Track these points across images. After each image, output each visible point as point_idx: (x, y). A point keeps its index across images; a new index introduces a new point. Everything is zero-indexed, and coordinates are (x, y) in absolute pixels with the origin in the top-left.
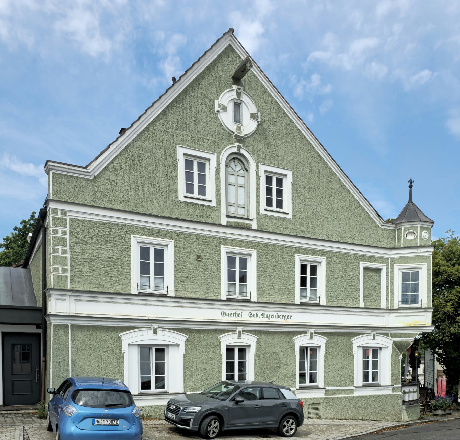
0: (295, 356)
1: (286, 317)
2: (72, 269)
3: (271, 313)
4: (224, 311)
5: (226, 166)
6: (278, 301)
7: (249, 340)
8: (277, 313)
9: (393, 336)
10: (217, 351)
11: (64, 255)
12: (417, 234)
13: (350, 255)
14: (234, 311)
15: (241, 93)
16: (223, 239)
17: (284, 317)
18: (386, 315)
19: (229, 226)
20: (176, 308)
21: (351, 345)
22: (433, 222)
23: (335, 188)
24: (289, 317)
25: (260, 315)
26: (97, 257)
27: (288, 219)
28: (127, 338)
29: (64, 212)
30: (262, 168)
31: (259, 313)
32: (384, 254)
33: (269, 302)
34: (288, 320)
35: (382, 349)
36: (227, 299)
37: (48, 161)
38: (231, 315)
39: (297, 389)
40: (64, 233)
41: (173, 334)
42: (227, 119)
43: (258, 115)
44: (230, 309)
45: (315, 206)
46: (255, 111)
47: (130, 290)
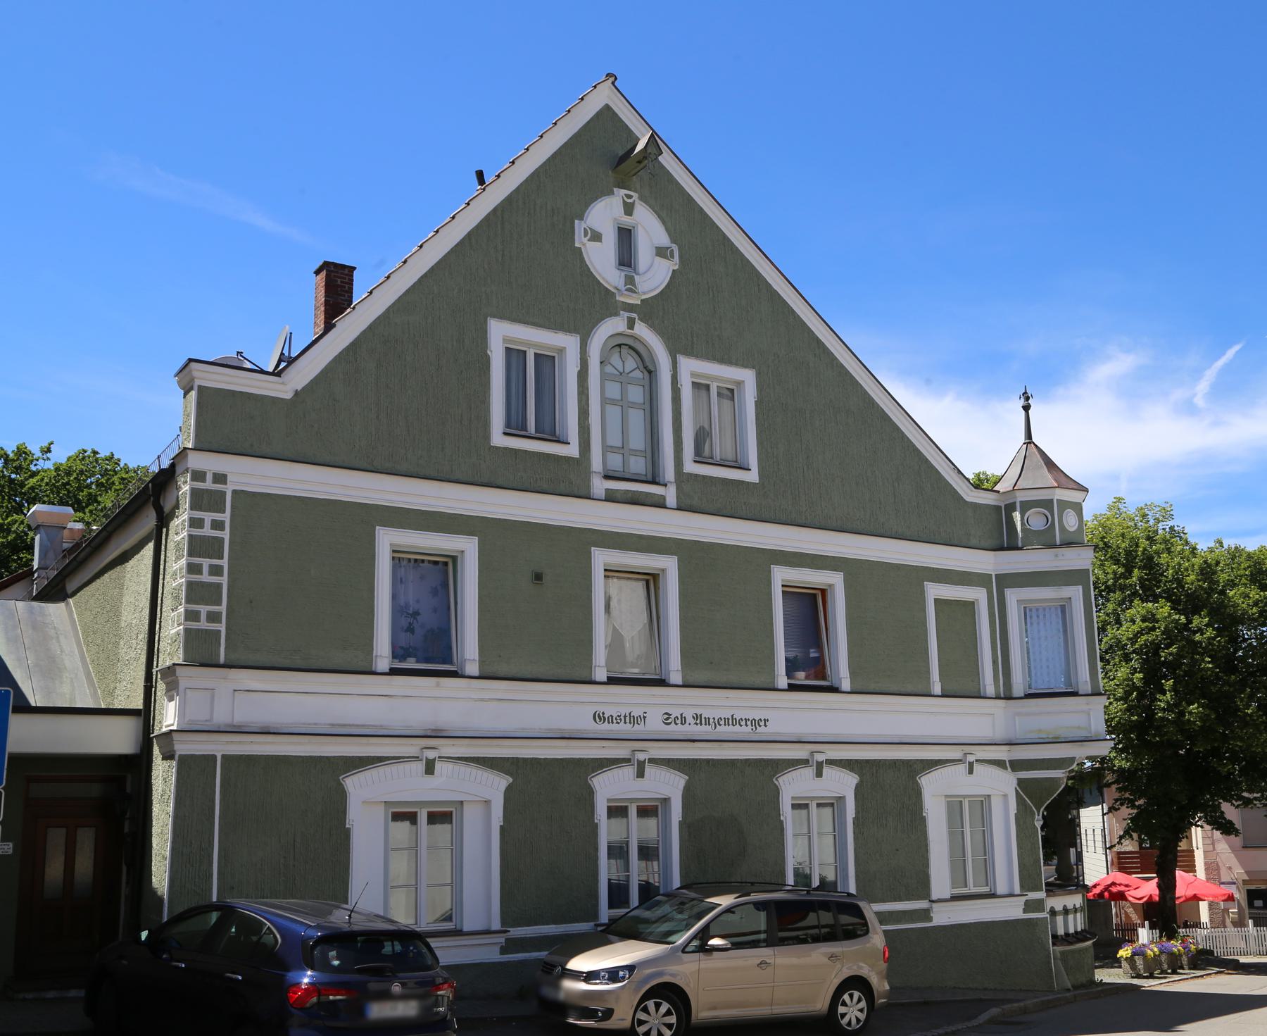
15: (633, 204)
19: (611, 497)
22: (1086, 490)
25: (690, 720)
29: (220, 478)
30: (690, 367)
36: (609, 678)
40: (216, 570)
42: (601, 260)
46: (663, 239)
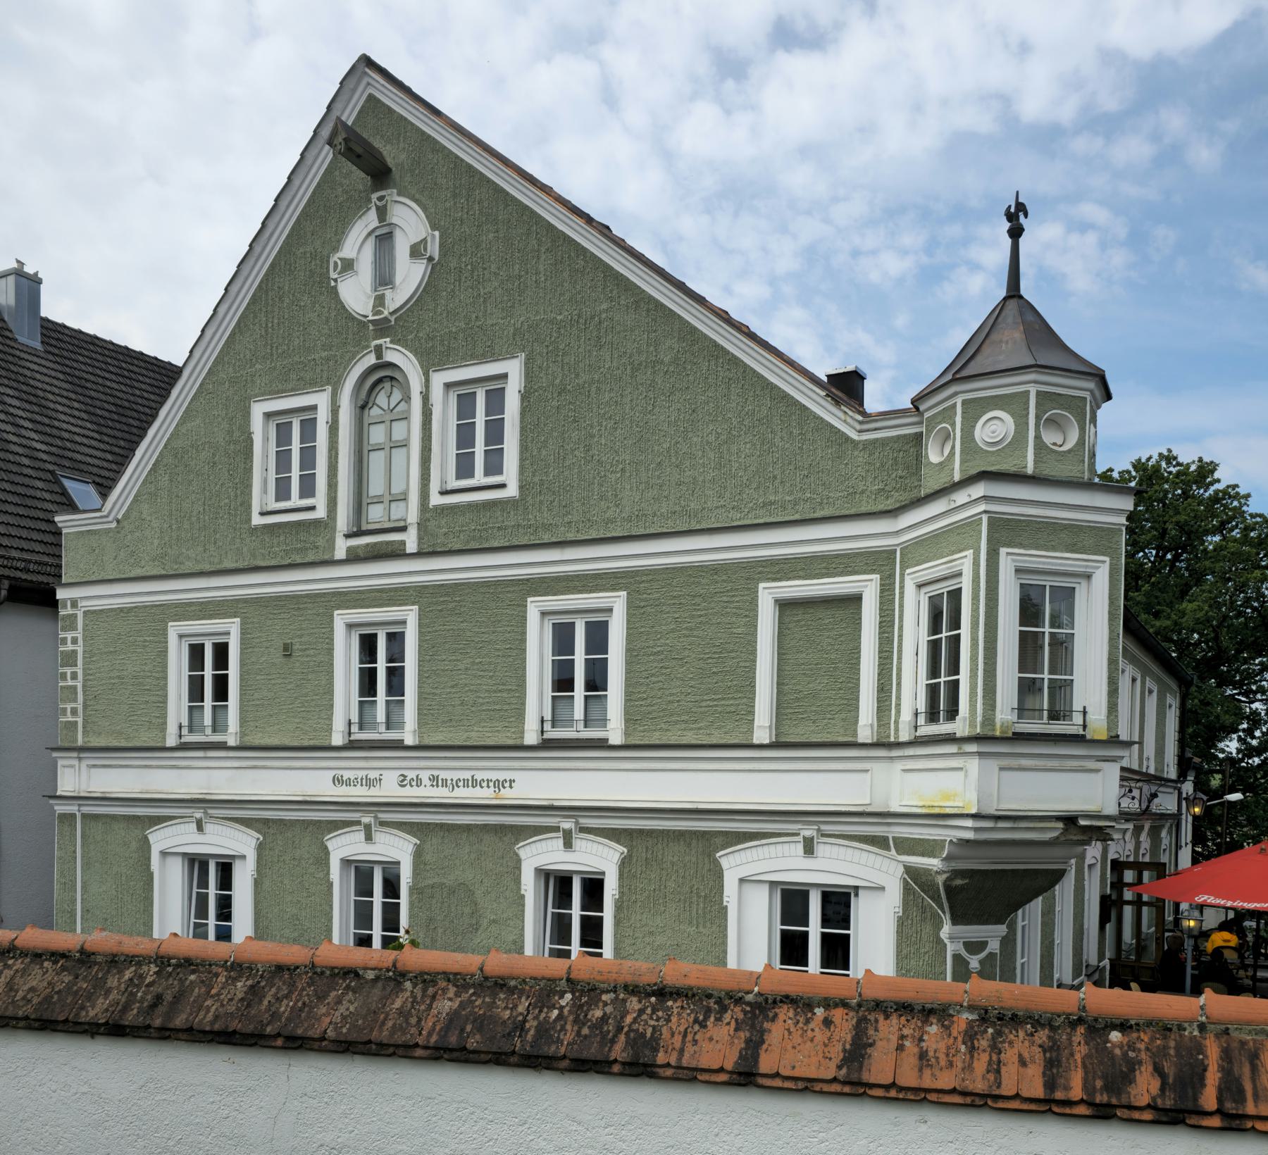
0: (523, 897)
1: (499, 784)
2: (85, 706)
3: (456, 775)
4: (340, 772)
6: (474, 738)
7: (240, 843)
8: (473, 773)
9: (906, 846)
10: (321, 875)
13: (715, 569)
14: (364, 773)
16: (340, 594)
17: (491, 784)
18: (876, 767)
19: (354, 557)
20: (242, 771)
21: (719, 874)
23: (667, 360)
24: (507, 785)
25: (426, 781)
26: (119, 677)
28: (160, 839)
31: (425, 776)
32: (410, 573)
33: (450, 743)
34: (506, 792)
35: (861, 892)
41: (772, 847)
44: (354, 766)
45: (592, 436)
47: (855, 734)
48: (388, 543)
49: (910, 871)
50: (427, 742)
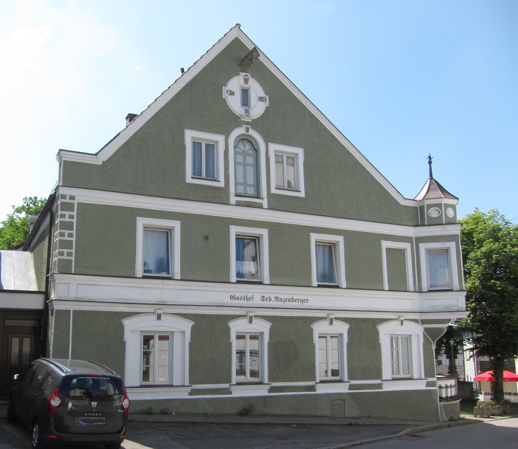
1: (302, 301)
5: (235, 147)
9: (423, 322)
11: (69, 258)
12: (442, 211)
15: (248, 79)
19: (238, 204)
24: (306, 301)
25: (273, 299)
27: (300, 198)
29: (72, 198)
30: (273, 147)
37: (60, 150)
38: (241, 298)
39: (316, 383)
40: (71, 235)
42: (235, 103)
43: (266, 99)
46: (262, 94)
48: (255, 203)
49: (426, 329)
50: (273, 283)
